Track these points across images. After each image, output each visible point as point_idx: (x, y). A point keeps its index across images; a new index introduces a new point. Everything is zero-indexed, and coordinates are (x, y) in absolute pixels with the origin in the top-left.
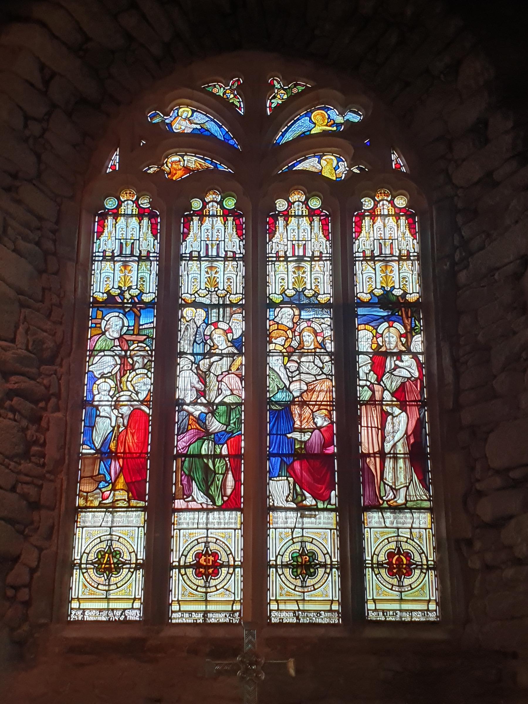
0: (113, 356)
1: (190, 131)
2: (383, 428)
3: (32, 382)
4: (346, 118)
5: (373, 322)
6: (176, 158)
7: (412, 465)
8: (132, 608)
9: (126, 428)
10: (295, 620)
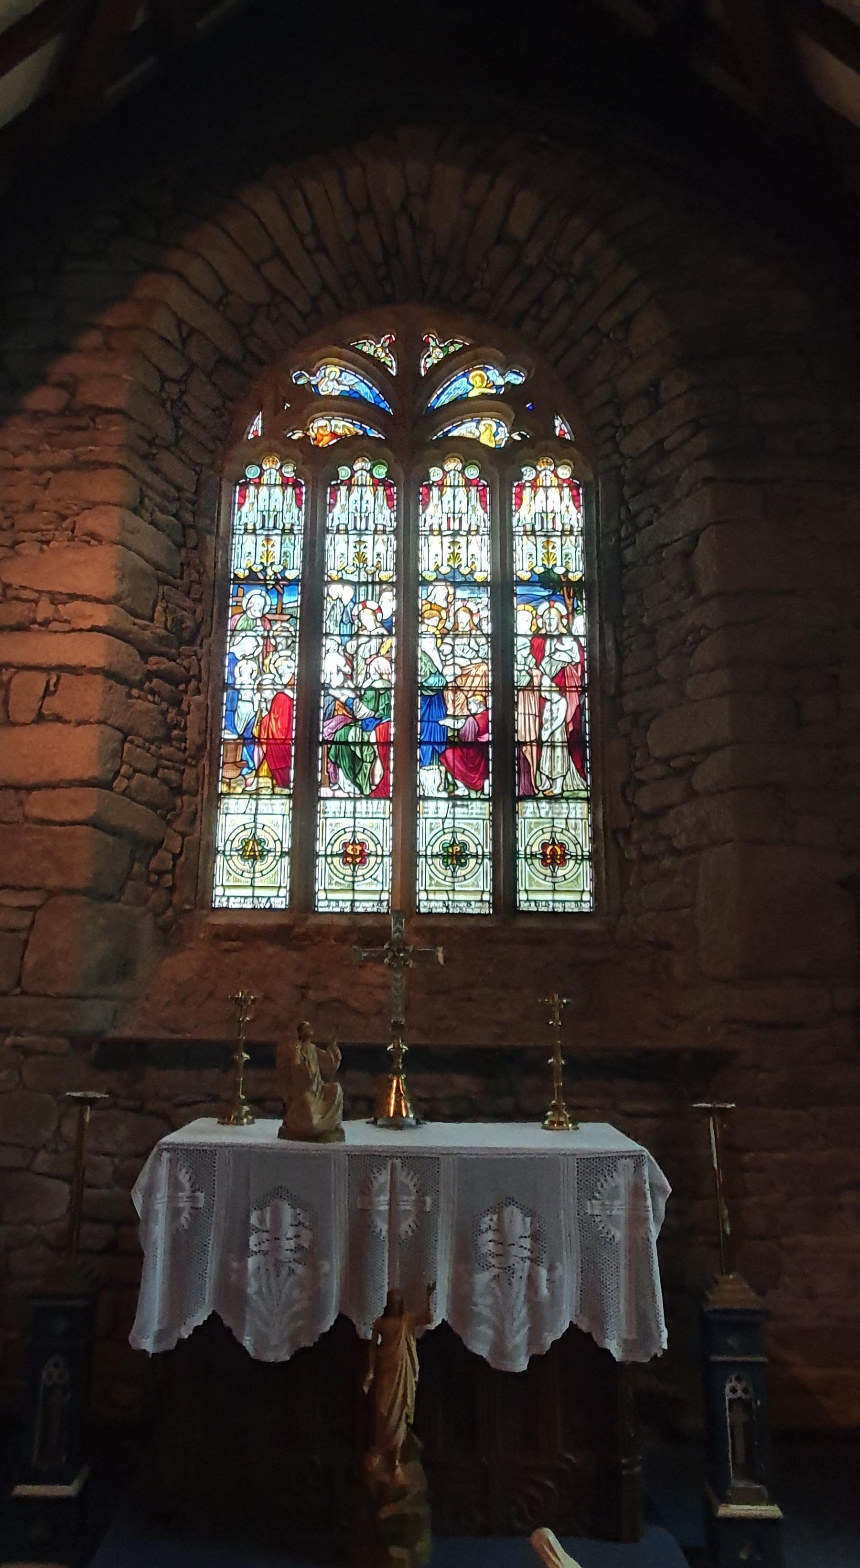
0: (255, 637)
1: (337, 393)
2: (540, 715)
3: (172, 663)
4: (507, 379)
5: (534, 601)
6: (322, 423)
7: (570, 753)
8: (278, 896)
9: (270, 713)
10: (444, 910)
